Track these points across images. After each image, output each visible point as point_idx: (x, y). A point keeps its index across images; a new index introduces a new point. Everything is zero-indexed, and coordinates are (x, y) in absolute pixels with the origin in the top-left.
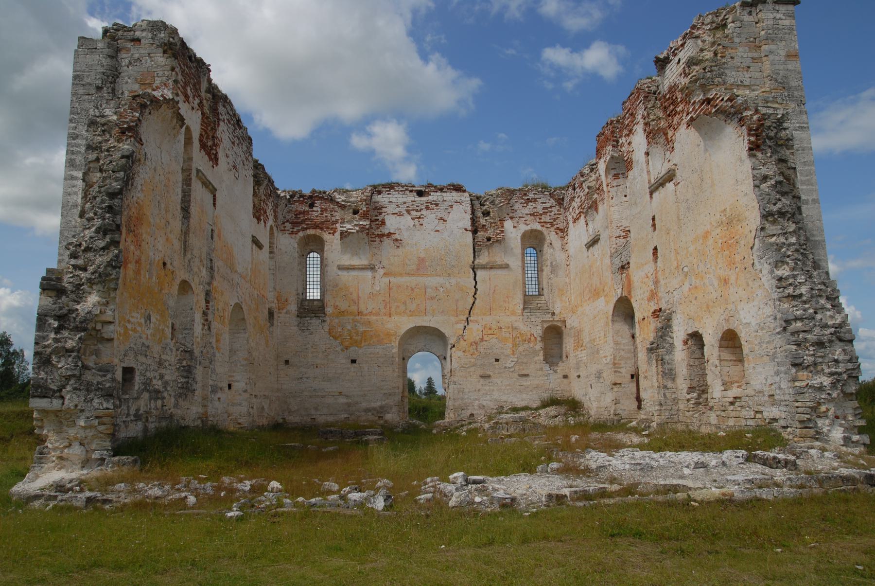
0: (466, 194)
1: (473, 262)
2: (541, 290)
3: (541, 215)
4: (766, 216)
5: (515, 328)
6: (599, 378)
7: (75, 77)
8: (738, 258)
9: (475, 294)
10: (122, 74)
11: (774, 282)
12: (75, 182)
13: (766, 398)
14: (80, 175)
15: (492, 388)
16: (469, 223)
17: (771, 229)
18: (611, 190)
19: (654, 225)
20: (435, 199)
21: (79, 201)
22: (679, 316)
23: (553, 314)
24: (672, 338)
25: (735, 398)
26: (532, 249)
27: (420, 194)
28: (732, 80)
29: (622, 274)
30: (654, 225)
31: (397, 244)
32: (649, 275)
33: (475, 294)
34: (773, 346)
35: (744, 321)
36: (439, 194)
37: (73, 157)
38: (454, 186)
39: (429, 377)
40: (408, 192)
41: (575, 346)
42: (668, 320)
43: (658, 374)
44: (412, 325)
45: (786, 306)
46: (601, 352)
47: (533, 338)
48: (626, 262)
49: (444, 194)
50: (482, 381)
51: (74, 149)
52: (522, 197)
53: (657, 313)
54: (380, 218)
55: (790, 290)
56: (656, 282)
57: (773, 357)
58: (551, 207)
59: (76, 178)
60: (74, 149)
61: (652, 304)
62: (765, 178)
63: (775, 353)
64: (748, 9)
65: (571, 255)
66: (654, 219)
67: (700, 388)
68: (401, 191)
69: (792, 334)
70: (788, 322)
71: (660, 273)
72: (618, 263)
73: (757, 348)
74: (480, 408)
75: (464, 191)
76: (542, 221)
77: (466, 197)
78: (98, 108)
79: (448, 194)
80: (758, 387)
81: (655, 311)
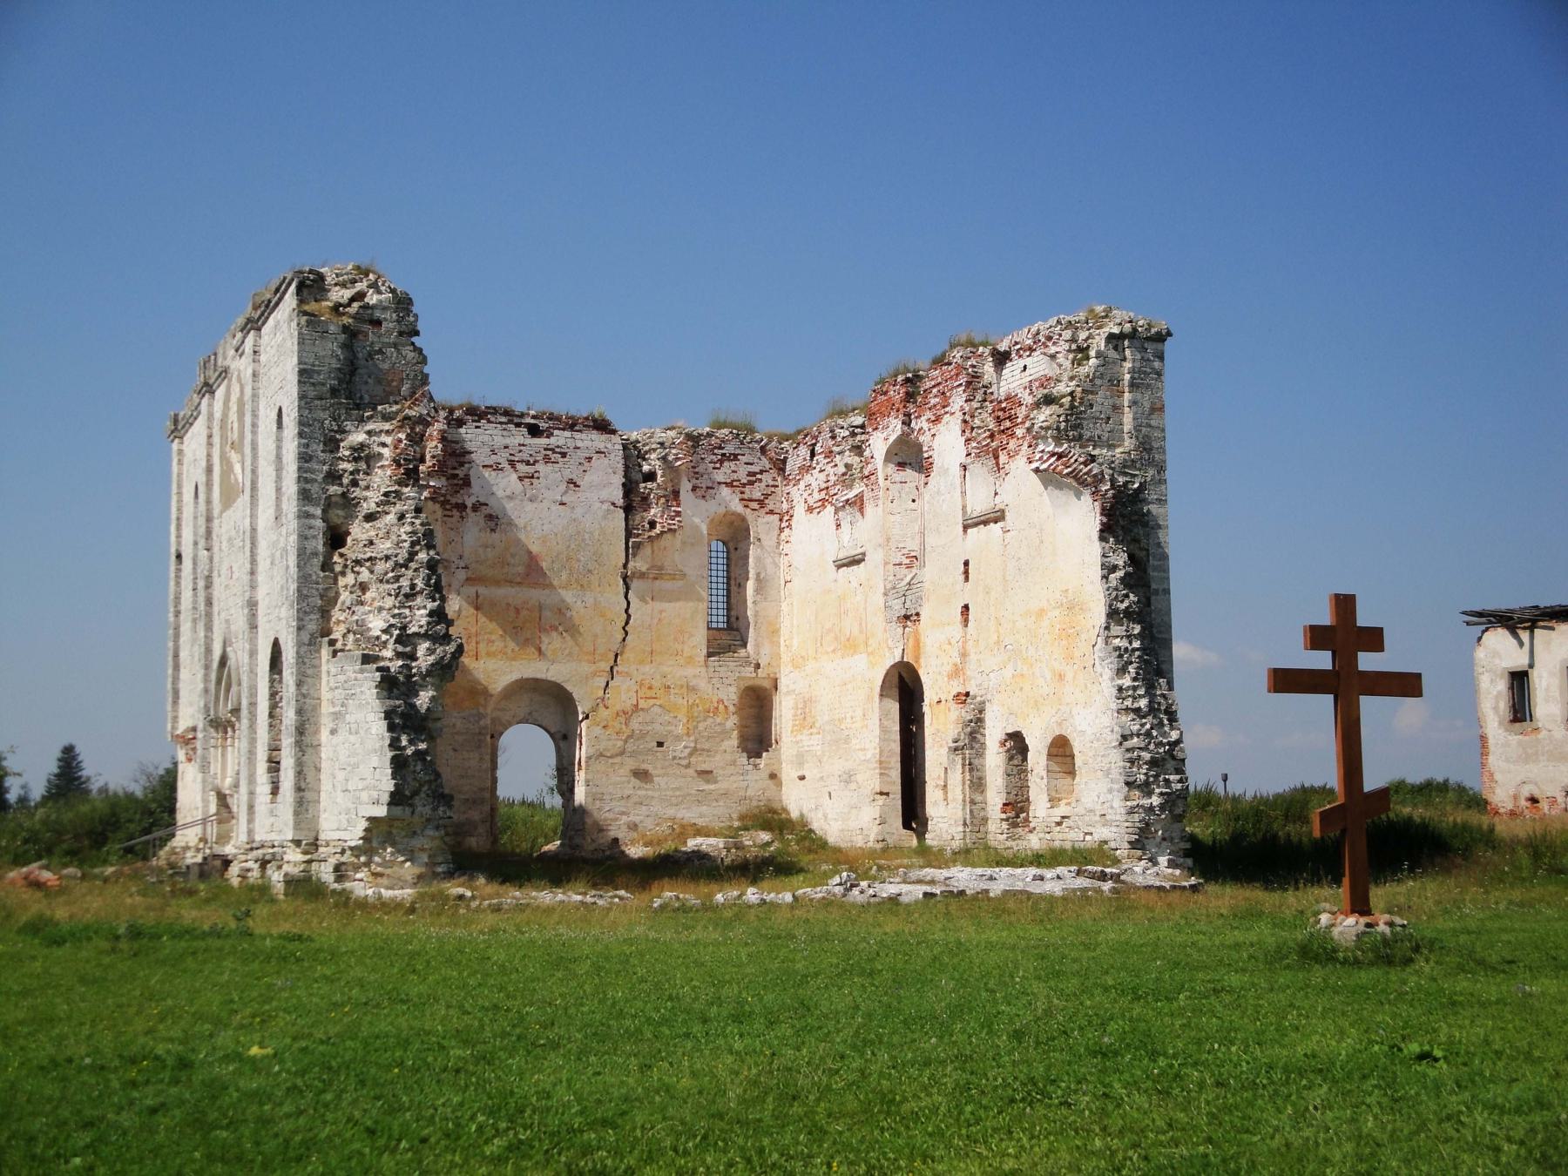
0: (616, 439)
1: (625, 566)
2: (733, 619)
3: (744, 485)
4: (1112, 614)
5: (692, 689)
6: (847, 782)
7: (302, 372)
8: (1077, 653)
9: (627, 623)
10: (360, 371)
11: (1114, 692)
12: (312, 522)
13: (1098, 818)
14: (319, 512)
15: (650, 793)
16: (621, 494)
17: (1117, 630)
18: (892, 487)
19: (966, 573)
20: (560, 444)
21: (321, 548)
22: (995, 708)
23: (758, 666)
24: (984, 735)
25: (1063, 817)
26: (720, 544)
27: (534, 431)
28: (1089, 434)
29: (904, 627)
30: (966, 573)
31: (492, 524)
32: (953, 641)
33: (627, 623)
34: (1106, 760)
35: (1079, 728)
36: (567, 434)
37: (308, 486)
38: (595, 420)
39: (66, 742)
40: (512, 427)
41: (794, 726)
42: (980, 712)
43: (964, 784)
44: (515, 676)
45: (1124, 718)
46: (854, 742)
47: (721, 707)
48: (914, 612)
49: (577, 435)
50: (635, 782)
51: (307, 475)
52: (712, 450)
53: (963, 697)
54: (461, 472)
55: (1128, 703)
56: (964, 655)
57: (1108, 773)
58: (761, 472)
59: (312, 516)
60: (307, 475)
61: (955, 683)
62: (1114, 568)
63: (1109, 769)
64: (1115, 342)
65: (795, 564)
66: (966, 563)
67: (1017, 808)
68: (501, 423)
69: (1128, 750)
70: (1125, 738)
71: (970, 643)
72: (898, 608)
73: (1091, 761)
74: (629, 827)
75: (614, 432)
76: (746, 496)
77: (614, 444)
78: (335, 420)
79: (583, 436)
80: (1089, 806)
81: (958, 694)
